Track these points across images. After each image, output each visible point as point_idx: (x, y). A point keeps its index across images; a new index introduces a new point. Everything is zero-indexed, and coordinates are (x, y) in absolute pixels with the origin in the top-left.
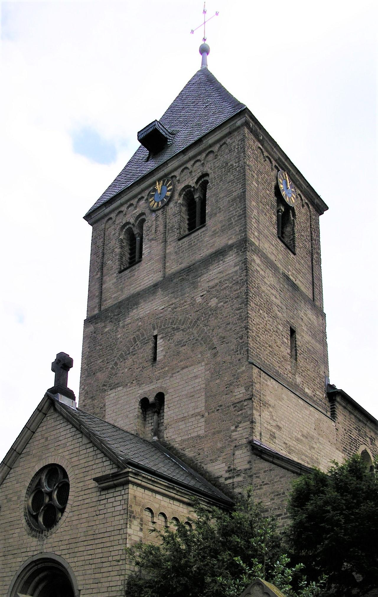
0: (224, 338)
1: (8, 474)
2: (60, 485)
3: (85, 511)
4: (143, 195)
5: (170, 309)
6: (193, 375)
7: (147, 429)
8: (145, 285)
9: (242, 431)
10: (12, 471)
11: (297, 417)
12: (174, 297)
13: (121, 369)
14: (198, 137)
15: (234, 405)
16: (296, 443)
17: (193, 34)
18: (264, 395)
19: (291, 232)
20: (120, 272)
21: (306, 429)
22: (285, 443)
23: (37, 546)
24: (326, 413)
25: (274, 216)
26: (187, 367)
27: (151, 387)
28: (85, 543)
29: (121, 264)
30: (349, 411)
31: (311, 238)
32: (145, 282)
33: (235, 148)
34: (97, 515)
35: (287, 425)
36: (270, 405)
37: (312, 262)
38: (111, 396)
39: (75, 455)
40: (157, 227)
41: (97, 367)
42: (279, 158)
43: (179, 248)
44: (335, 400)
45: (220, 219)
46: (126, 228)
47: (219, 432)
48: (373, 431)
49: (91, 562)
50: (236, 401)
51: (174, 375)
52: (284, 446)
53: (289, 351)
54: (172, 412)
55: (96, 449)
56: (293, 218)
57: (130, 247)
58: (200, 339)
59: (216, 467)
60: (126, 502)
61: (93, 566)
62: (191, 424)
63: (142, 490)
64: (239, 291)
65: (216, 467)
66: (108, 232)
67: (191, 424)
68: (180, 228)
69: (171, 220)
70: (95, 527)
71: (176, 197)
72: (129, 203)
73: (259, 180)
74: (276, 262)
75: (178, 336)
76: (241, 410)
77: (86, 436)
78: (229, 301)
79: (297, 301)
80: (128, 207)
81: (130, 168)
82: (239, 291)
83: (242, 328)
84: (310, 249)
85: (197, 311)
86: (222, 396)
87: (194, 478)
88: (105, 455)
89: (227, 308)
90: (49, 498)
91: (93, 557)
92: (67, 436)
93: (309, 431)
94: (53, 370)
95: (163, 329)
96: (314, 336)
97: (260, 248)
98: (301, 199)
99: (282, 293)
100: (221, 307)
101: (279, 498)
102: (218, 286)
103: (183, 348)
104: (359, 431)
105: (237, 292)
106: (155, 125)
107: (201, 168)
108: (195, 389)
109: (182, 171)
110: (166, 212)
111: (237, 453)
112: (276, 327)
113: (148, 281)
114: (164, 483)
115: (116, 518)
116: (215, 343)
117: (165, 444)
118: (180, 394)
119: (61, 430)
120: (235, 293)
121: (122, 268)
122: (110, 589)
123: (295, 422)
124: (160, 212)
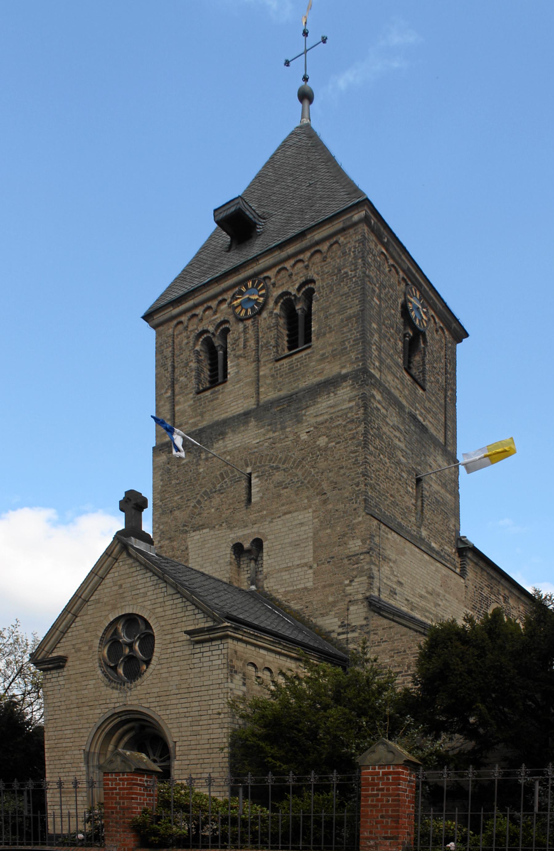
0: (336, 483)
1: (73, 622)
2: (142, 636)
3: (176, 664)
4: (225, 296)
5: (267, 444)
6: (298, 522)
7: (242, 577)
8: (233, 412)
9: (358, 586)
10: (78, 619)
11: (421, 573)
12: (271, 430)
13: (205, 508)
14: (300, 229)
15: (349, 557)
16: (419, 600)
17: (288, 67)
18: (384, 549)
19: (421, 362)
20: (198, 393)
21: (431, 585)
22: (407, 600)
23: (119, 697)
24: (454, 570)
25: (400, 343)
26: (290, 512)
27: (247, 531)
28: (179, 696)
29: (199, 382)
30: (482, 568)
31: (446, 371)
32: (232, 408)
33: (350, 250)
34: (191, 669)
35: (409, 581)
36: (390, 560)
37: (445, 401)
38: (195, 538)
39: (159, 605)
40: (246, 341)
41: (174, 504)
42: (408, 268)
43: (277, 370)
44: (466, 556)
45: (331, 340)
46: (203, 337)
47: (331, 585)
48: (507, 589)
49: (187, 714)
50: (350, 554)
51: (274, 520)
52: (406, 602)
53: (413, 501)
54: (273, 560)
55: (184, 600)
56: (424, 345)
57: (209, 362)
58: (306, 482)
59: (327, 622)
60: (226, 657)
61: (190, 719)
62: (296, 575)
63: (244, 645)
64: (355, 431)
65: (327, 622)
66: (179, 339)
67: (296, 575)
68: (277, 346)
69: (264, 334)
70: (189, 681)
71: (271, 304)
72: (205, 305)
73: (382, 296)
74: (400, 399)
75: (278, 476)
76: (357, 564)
77: (172, 586)
78: (343, 441)
79: (425, 445)
80: (205, 311)
81: (204, 257)
82: (355, 431)
83: (358, 473)
84: (444, 384)
85: (302, 450)
86: (334, 547)
87: (301, 631)
88: (196, 607)
89: (340, 450)
90: (130, 649)
91: (189, 710)
92: (147, 585)
93: (434, 587)
94: (122, 509)
95: (259, 467)
96: (444, 486)
97: (382, 381)
98: (435, 322)
99: (407, 436)
100: (332, 448)
101: (399, 656)
102: (328, 422)
103: (285, 490)
104: (492, 588)
105: (352, 432)
106: (238, 203)
107: (305, 271)
108: (301, 538)
109: (279, 272)
110: (258, 323)
111: (352, 608)
112: (400, 474)
113: (236, 407)
114: (269, 638)
115: (214, 672)
116: (326, 488)
117: (265, 595)
118: (282, 542)
119: (139, 578)
120: (350, 433)
121: (201, 388)
122: (211, 741)
123: (419, 578)
124: (249, 323)
